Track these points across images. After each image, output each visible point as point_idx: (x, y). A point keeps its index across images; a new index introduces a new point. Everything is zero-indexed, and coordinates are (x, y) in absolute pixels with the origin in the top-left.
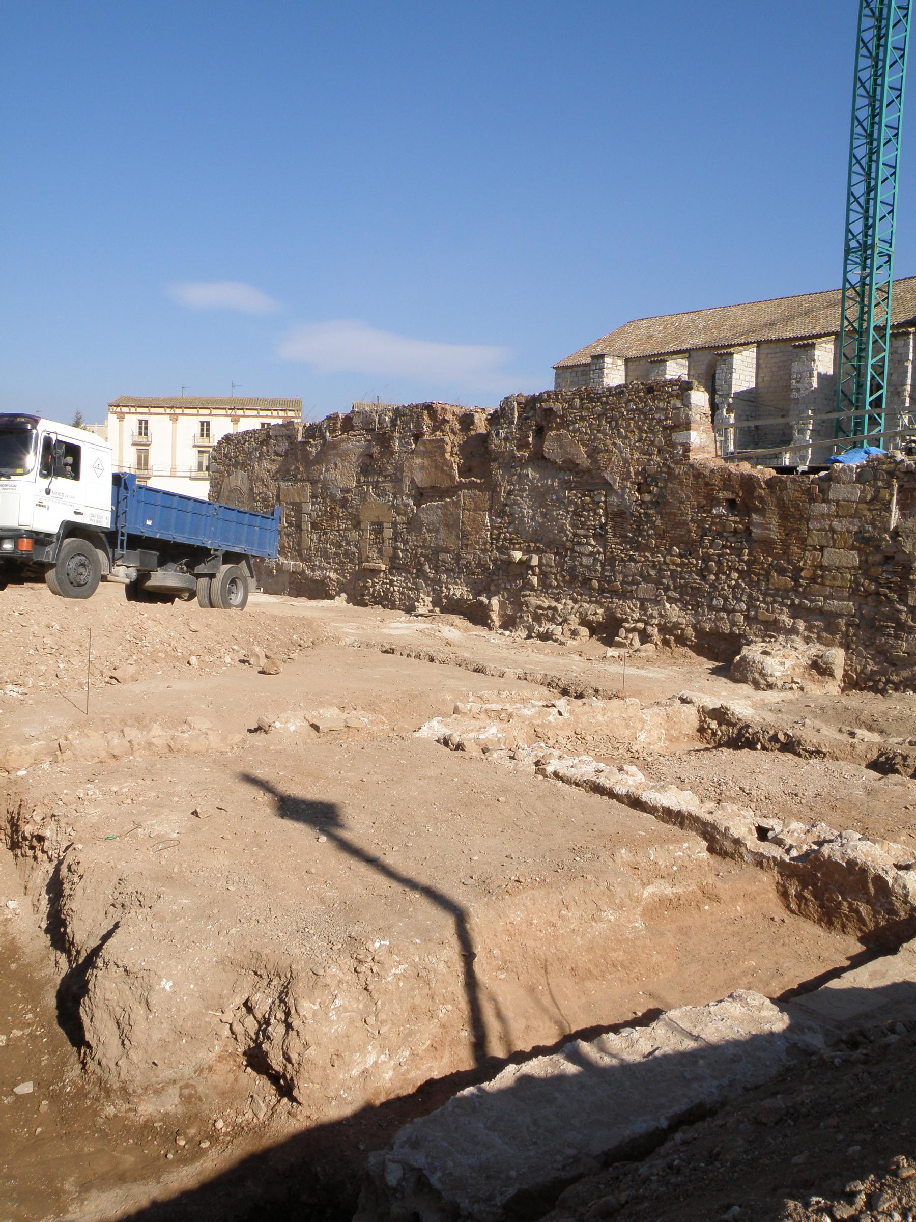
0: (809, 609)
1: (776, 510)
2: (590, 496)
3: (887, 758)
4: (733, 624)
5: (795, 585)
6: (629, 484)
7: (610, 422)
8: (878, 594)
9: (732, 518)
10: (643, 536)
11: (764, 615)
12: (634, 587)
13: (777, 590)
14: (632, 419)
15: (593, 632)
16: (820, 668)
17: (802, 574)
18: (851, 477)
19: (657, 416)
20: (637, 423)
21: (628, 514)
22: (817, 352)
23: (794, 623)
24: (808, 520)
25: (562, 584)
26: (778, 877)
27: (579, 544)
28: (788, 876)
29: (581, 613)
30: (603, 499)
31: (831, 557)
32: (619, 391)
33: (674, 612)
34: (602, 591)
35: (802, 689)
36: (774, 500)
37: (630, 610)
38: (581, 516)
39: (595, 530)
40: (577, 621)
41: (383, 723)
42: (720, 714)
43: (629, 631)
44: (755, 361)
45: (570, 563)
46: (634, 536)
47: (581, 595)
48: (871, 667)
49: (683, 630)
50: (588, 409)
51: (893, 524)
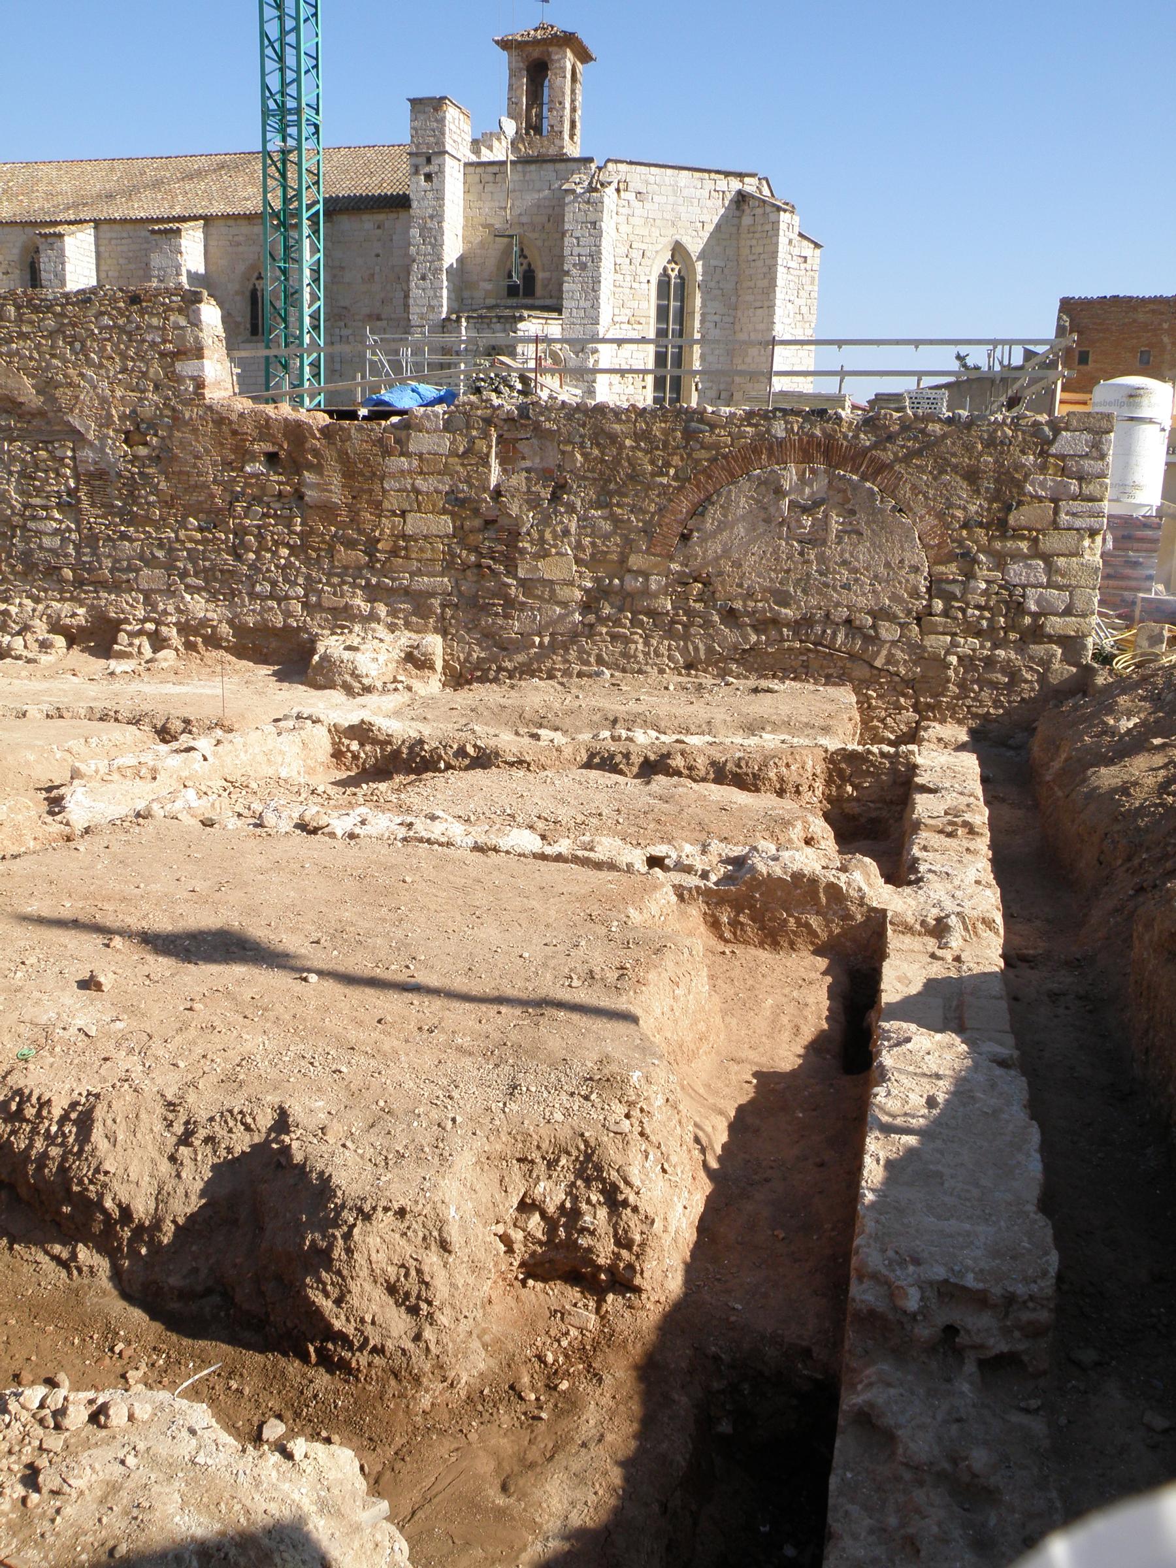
0: (390, 591)
1: (338, 466)
2: (47, 450)
3: (602, 758)
4: (288, 614)
5: (370, 561)
6: (111, 433)
7: (71, 344)
8: (479, 566)
9: (276, 478)
10: (140, 506)
11: (329, 600)
12: (132, 575)
13: (346, 568)
14: (108, 340)
15: (71, 641)
16: (416, 660)
17: (380, 546)
18: (437, 424)
19: (149, 338)
20: (118, 347)
21: (113, 473)
22: (183, 242)
23: (372, 608)
24: (382, 479)
25: (11, 577)
26: (704, 907)
27: (34, 518)
28: (717, 904)
29: (49, 616)
30: (69, 453)
31: (415, 523)
32: (85, 298)
33: (198, 606)
34: (79, 583)
35: (409, 689)
36: (335, 454)
37: (130, 607)
38: (34, 479)
39: (60, 497)
40: (45, 627)
41: (28, 808)
42: (362, 732)
43: (131, 635)
44: (93, 248)
45: (21, 546)
46: (125, 504)
47: (45, 590)
48: (477, 653)
49: (214, 628)
50: (31, 322)
51: (493, 482)
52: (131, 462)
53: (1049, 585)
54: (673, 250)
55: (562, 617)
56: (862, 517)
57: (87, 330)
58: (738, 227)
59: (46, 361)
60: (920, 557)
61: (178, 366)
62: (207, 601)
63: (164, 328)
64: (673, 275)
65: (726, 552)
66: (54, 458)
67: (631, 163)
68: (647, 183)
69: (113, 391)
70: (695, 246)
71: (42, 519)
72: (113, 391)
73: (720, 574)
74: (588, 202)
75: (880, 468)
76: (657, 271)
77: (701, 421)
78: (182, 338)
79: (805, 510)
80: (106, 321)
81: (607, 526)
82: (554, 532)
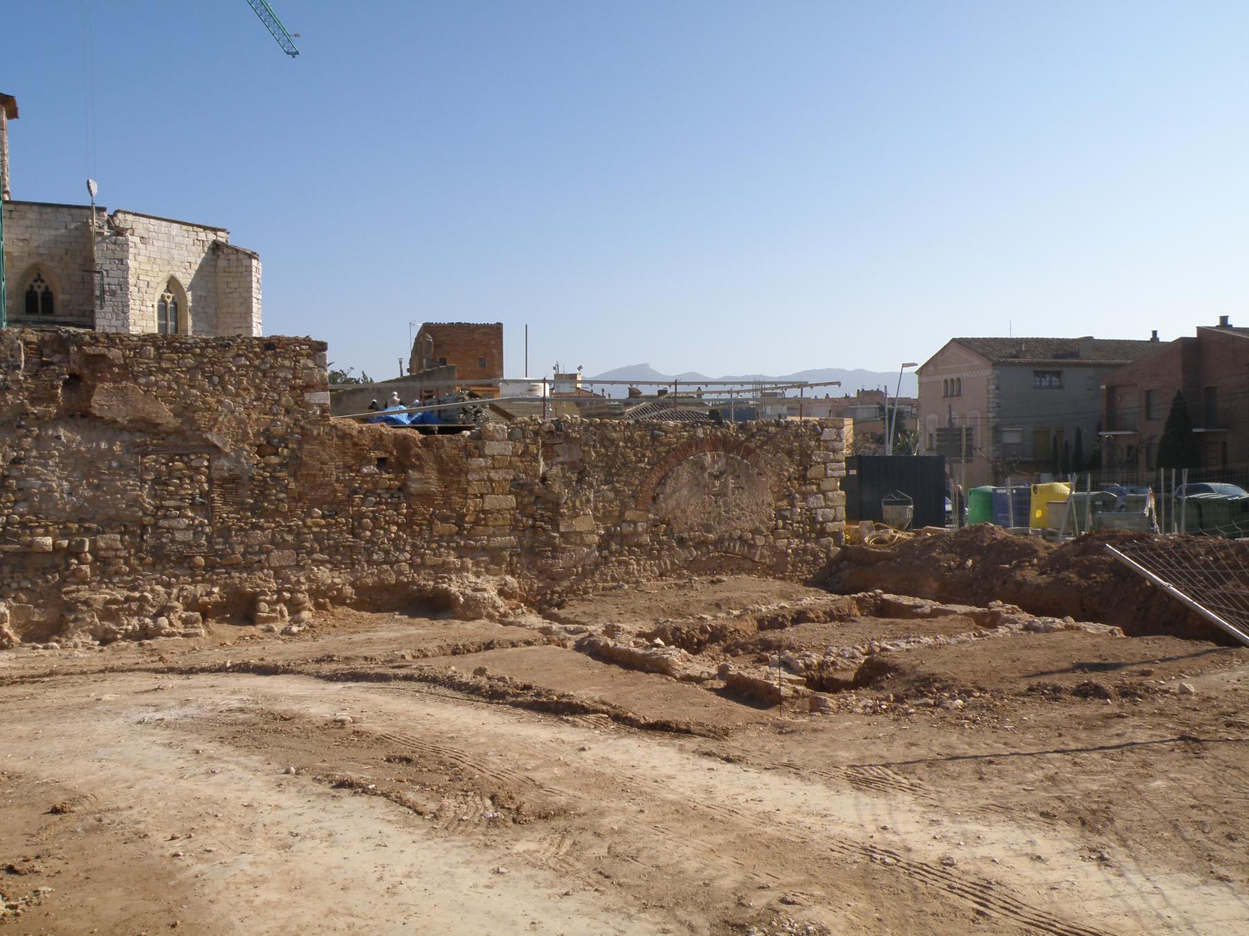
0: (474, 549)
1: (435, 466)
4: (400, 573)
7: (210, 378)
10: (271, 502)
11: (430, 559)
12: (263, 557)
13: (441, 536)
21: (246, 478)
23: (463, 563)
25: (140, 568)
27: (165, 517)
30: (206, 463)
31: (490, 502)
32: (148, 339)
33: (324, 574)
34: (211, 567)
39: (193, 499)
45: (152, 541)
46: (256, 501)
50: (171, 360)
52: (263, 468)
53: (827, 507)
54: (169, 283)
55: (588, 555)
56: (743, 479)
57: (225, 367)
58: (215, 266)
59: (184, 390)
60: (769, 498)
61: (307, 396)
62: (331, 570)
63: (295, 368)
64: (169, 301)
65: (678, 504)
66: (189, 468)
67: (136, 214)
68: (148, 231)
69: (249, 415)
70: (185, 280)
71: (175, 517)
72: (249, 415)
73: (675, 518)
74: (115, 243)
75: (749, 452)
76: (158, 297)
77: (660, 429)
78: (311, 376)
79: (716, 477)
80: (243, 361)
81: (611, 495)
82: (581, 501)
